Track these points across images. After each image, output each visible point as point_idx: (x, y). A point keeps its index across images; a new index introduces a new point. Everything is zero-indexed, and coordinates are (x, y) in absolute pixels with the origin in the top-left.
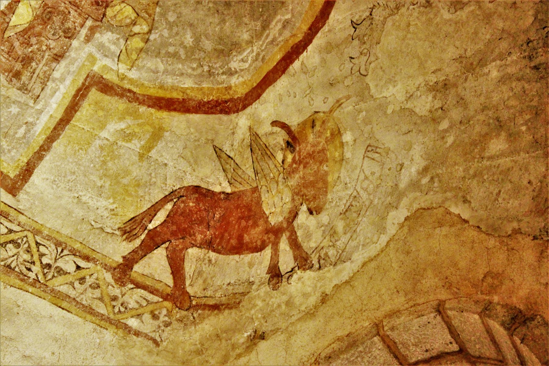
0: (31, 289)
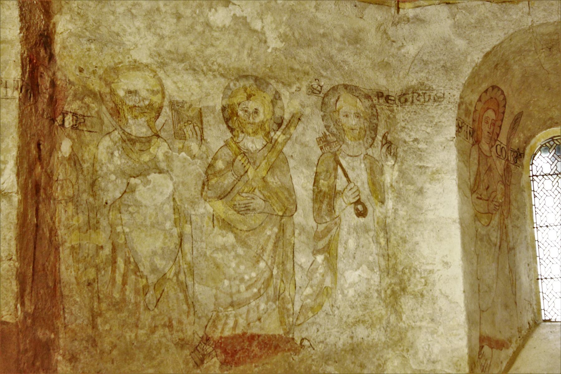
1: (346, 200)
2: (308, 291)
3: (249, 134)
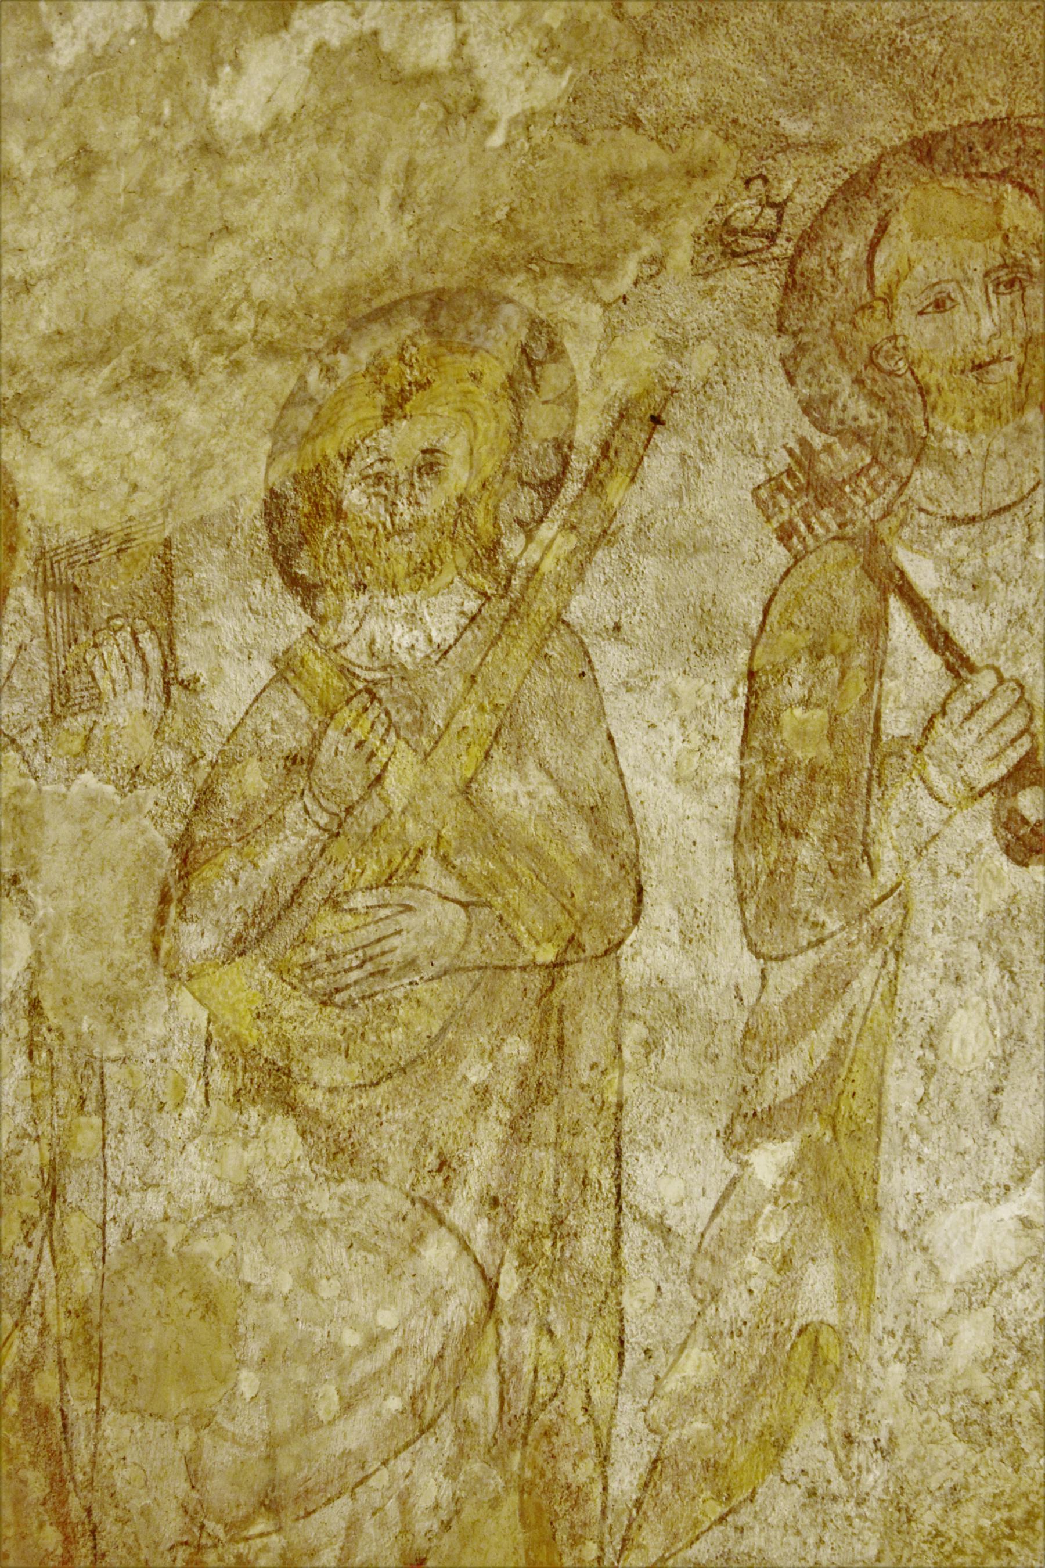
1: (941, 785)
2: (695, 1365)
3: (393, 587)
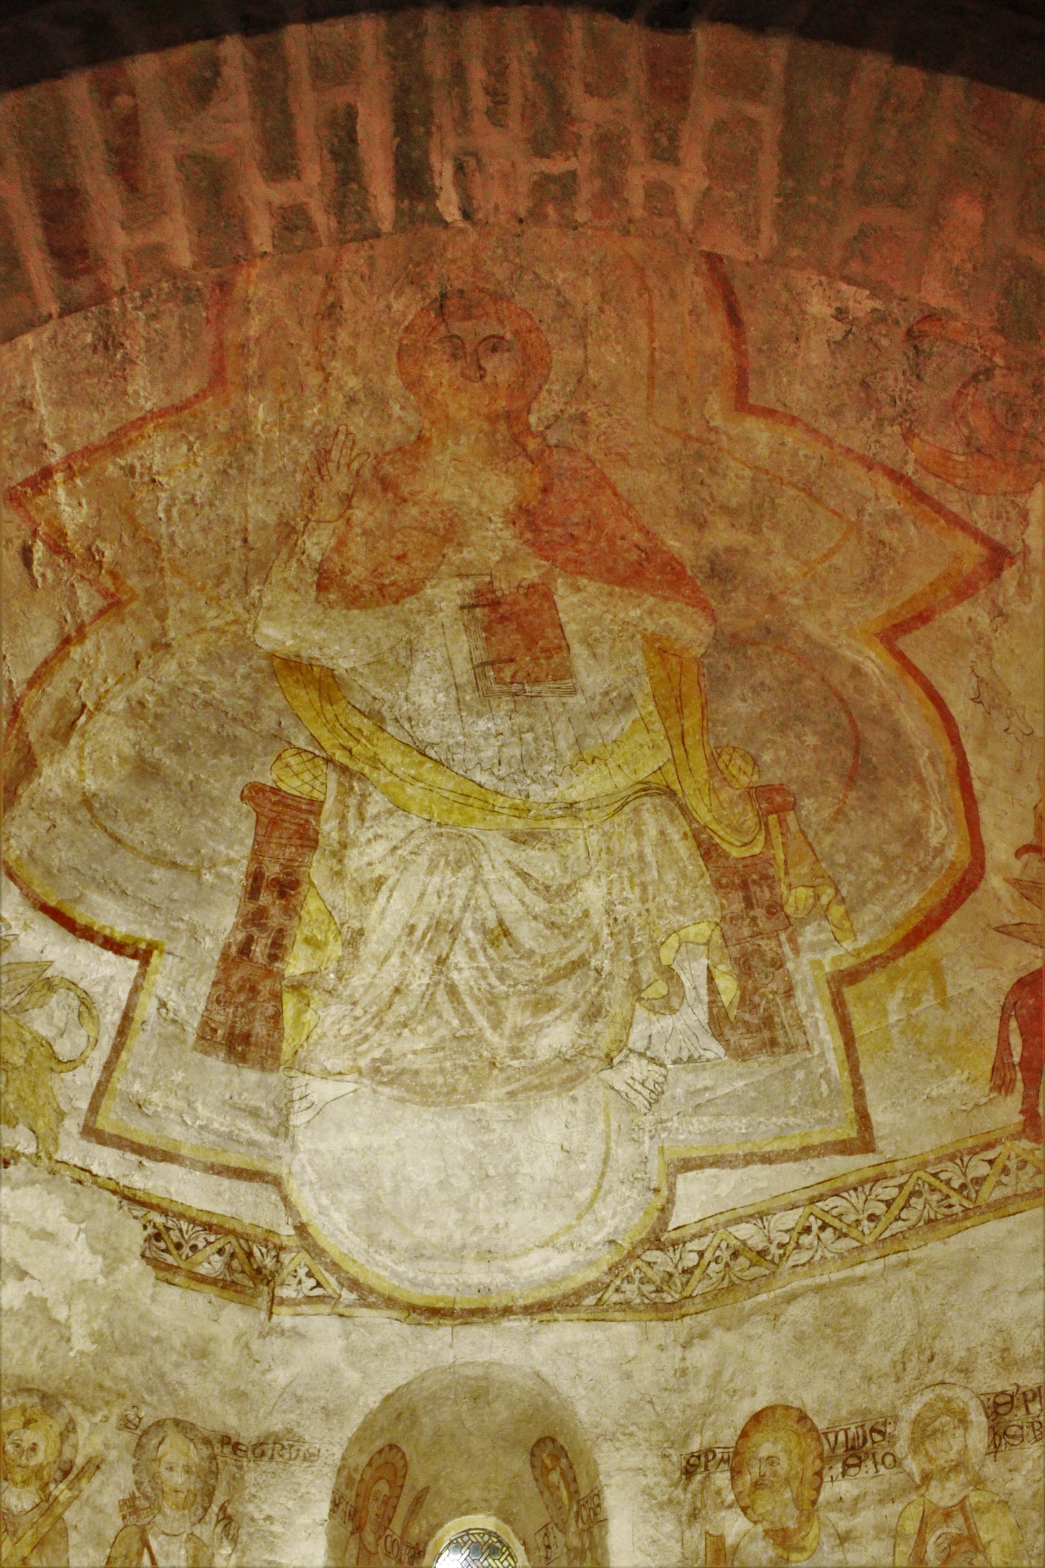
0: (968, 1223)
3: (15, 1484)
